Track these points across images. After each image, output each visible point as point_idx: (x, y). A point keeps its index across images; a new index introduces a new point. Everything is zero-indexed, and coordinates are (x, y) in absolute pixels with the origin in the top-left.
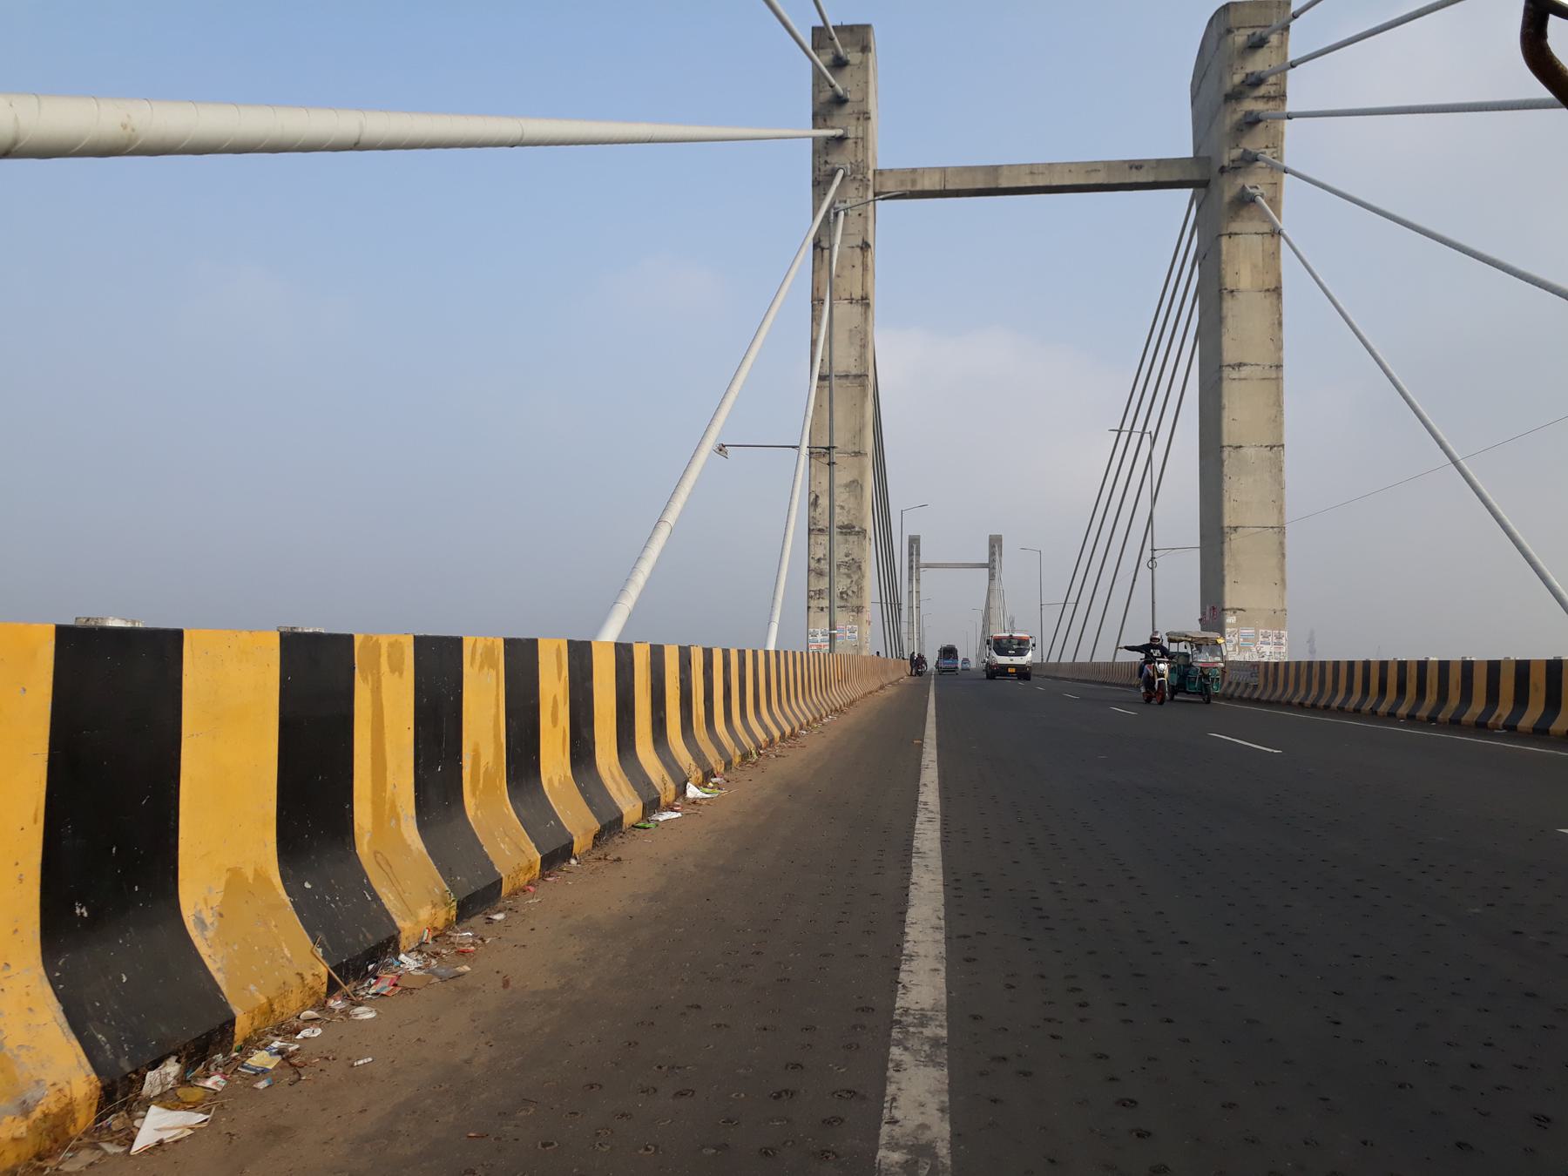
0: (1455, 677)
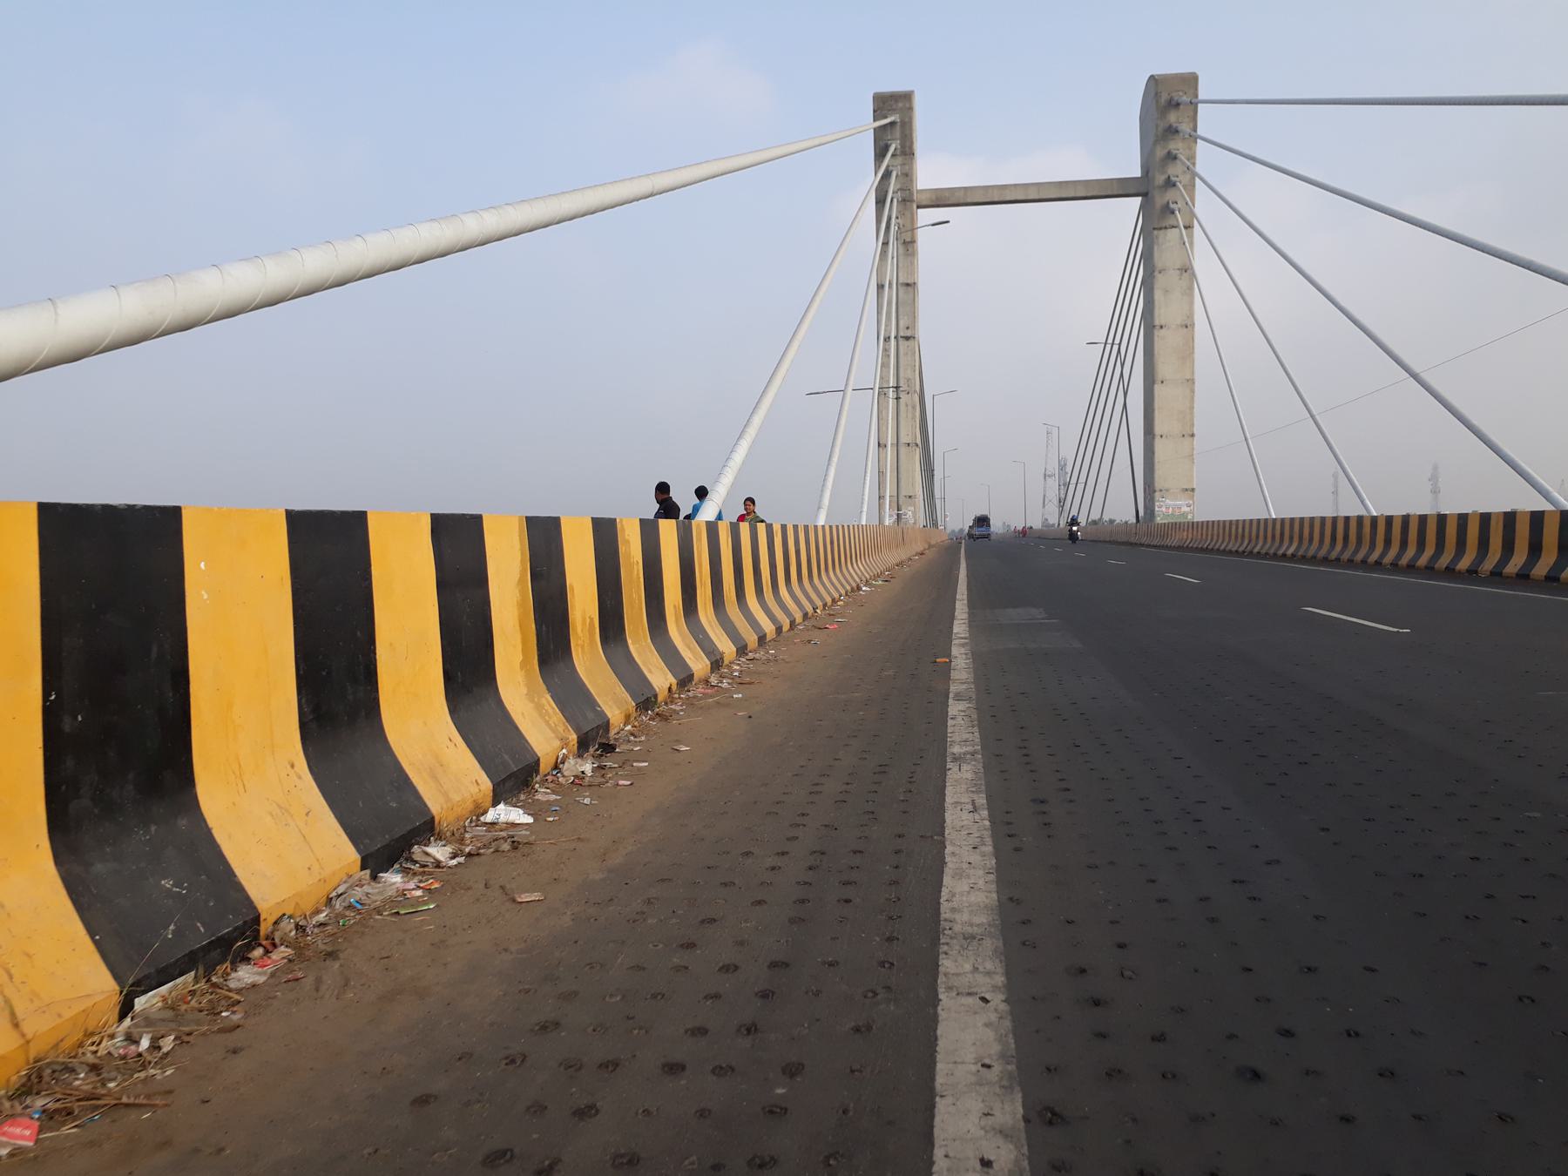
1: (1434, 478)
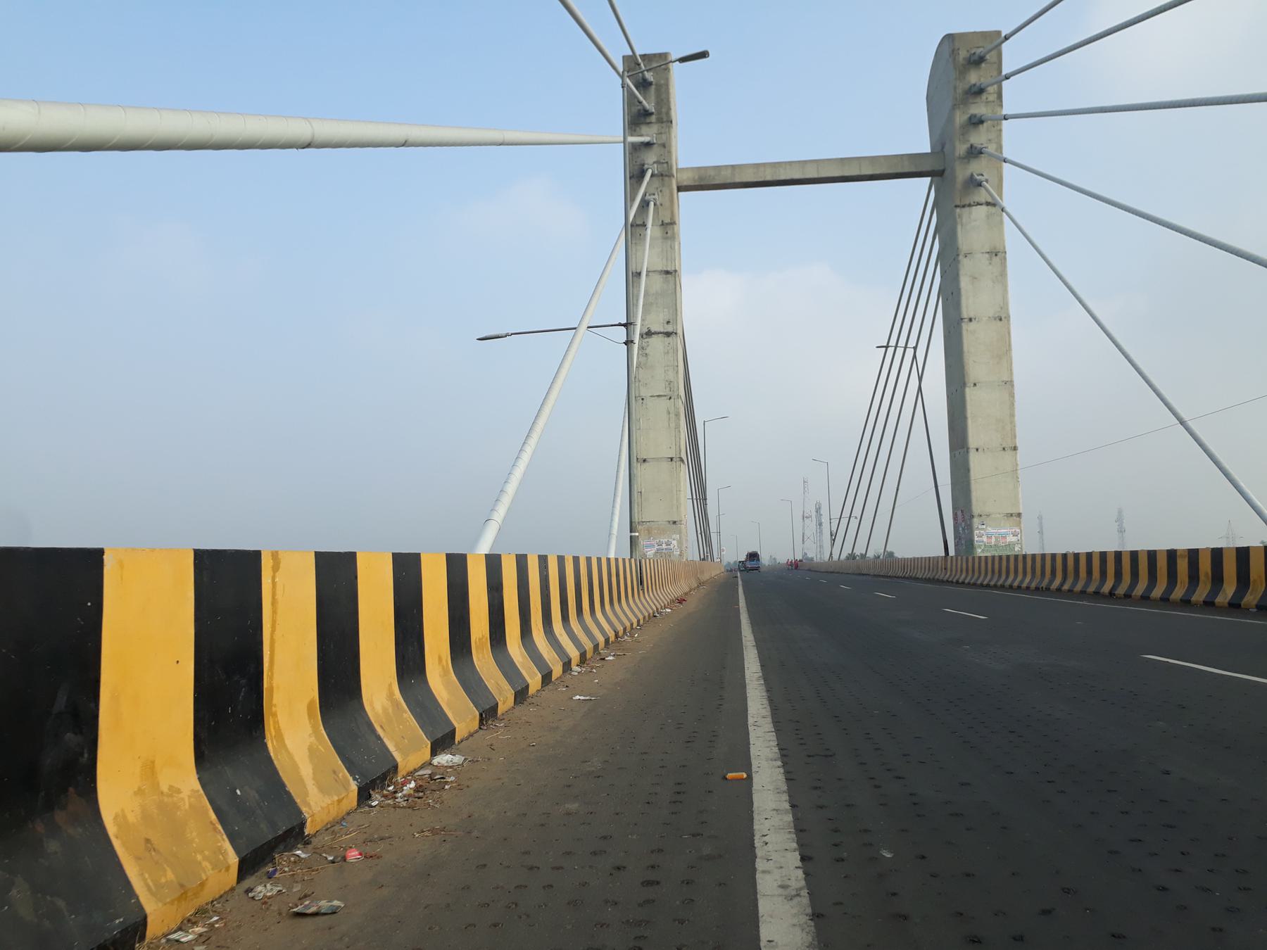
0: (1162, 564)
1: (1120, 520)
